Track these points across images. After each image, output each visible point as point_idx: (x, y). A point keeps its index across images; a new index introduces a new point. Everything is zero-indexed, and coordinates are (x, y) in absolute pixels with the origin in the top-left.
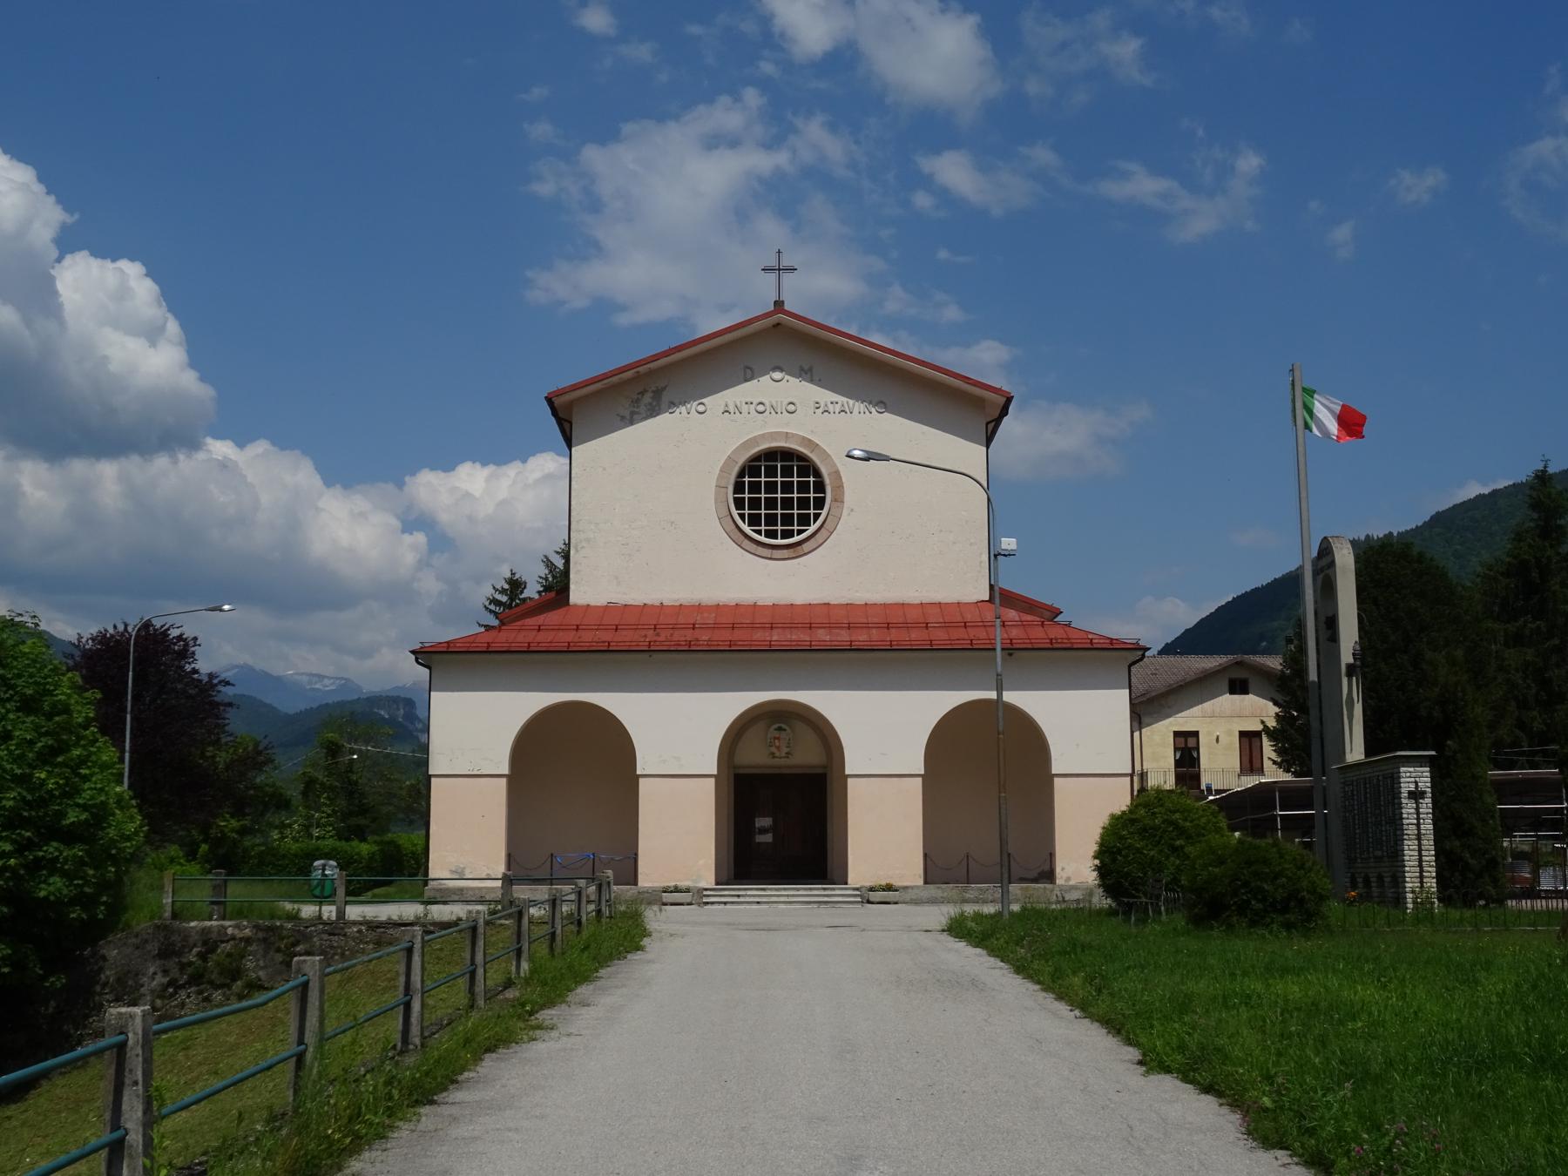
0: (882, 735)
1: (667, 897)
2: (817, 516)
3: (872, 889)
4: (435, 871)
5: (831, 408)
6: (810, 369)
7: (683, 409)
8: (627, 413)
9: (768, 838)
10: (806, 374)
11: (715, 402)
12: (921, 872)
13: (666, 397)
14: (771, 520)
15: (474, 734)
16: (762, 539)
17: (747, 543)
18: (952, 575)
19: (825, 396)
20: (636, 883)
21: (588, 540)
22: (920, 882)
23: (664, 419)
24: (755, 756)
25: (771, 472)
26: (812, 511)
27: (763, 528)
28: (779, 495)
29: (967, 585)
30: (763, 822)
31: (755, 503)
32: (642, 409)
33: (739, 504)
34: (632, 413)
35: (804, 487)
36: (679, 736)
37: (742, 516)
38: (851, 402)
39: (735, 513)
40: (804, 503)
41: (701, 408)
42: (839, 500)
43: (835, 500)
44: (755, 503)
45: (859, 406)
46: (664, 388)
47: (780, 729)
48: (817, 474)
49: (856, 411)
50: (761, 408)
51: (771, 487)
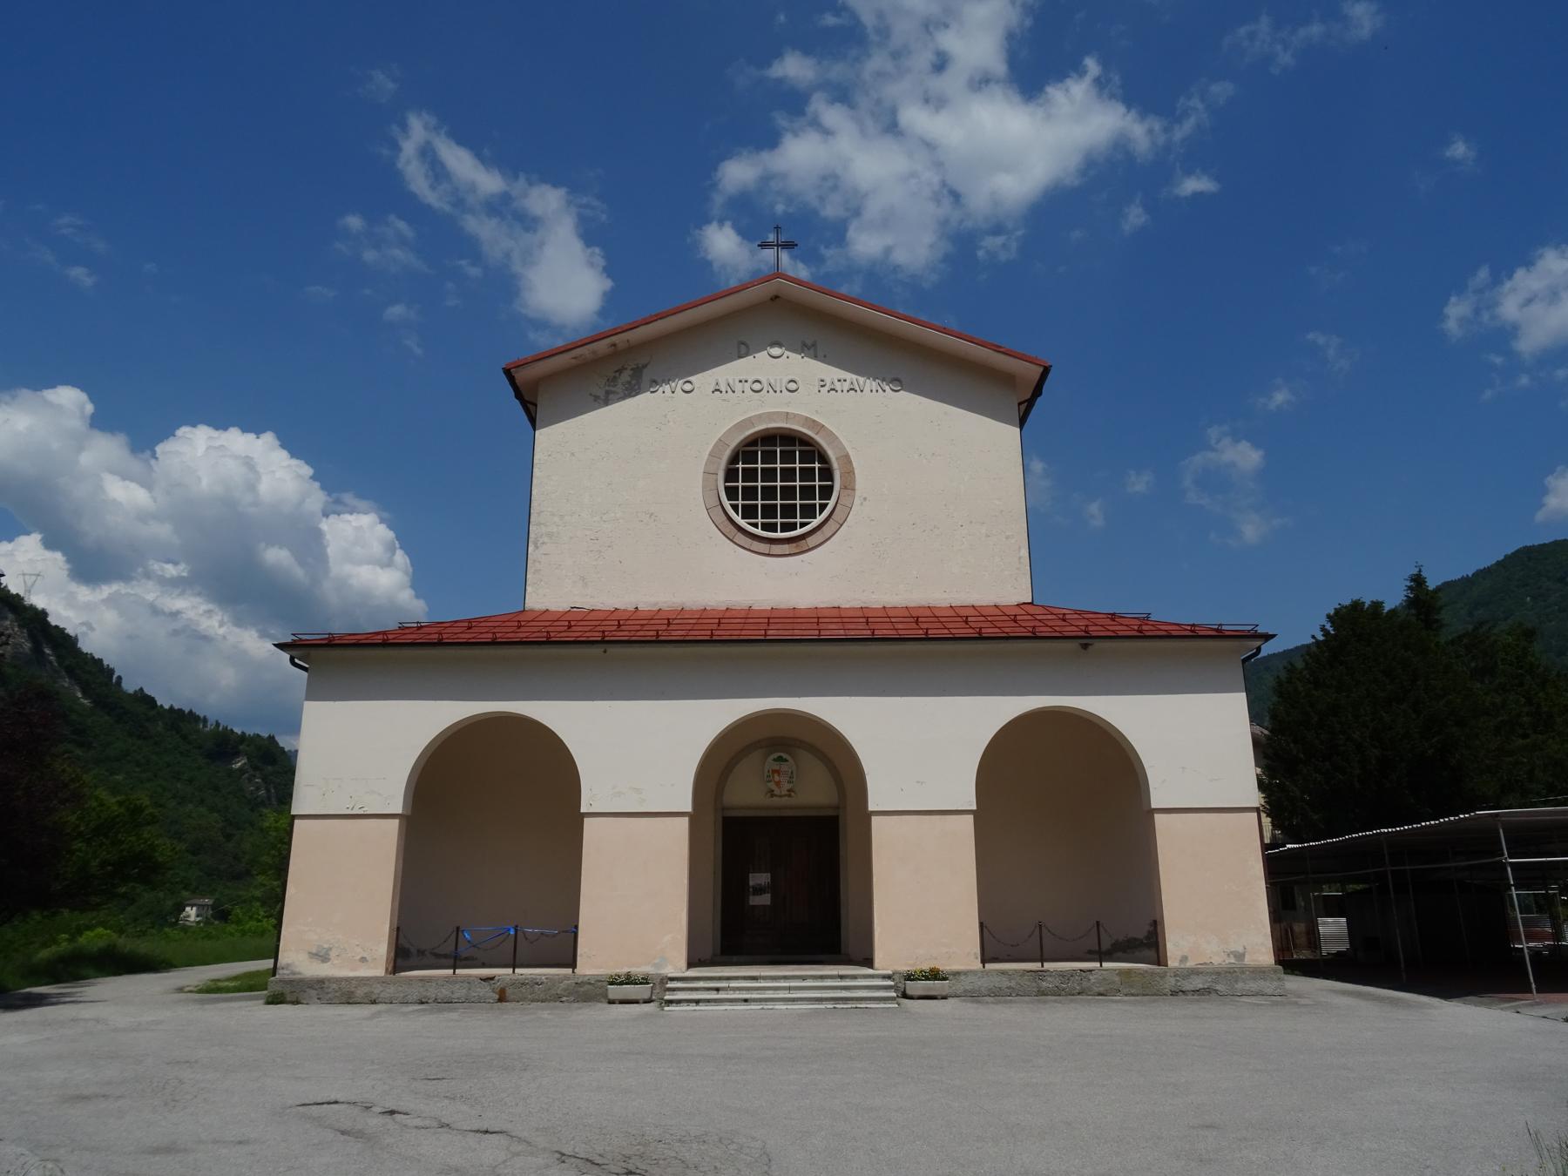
0: (919, 757)
1: (615, 991)
2: (823, 507)
3: (909, 977)
5: (838, 386)
6: (814, 345)
7: (667, 388)
8: (601, 393)
9: (765, 900)
10: (808, 349)
11: (703, 381)
12: (978, 950)
13: (647, 375)
14: (769, 511)
15: (358, 759)
16: (759, 532)
17: (740, 538)
18: (988, 569)
19: (832, 373)
20: (573, 965)
21: (550, 535)
23: (643, 400)
24: (749, 793)
25: (769, 457)
26: (817, 502)
27: (760, 520)
28: (779, 482)
30: (760, 878)
31: (750, 493)
32: (619, 388)
33: (731, 493)
34: (608, 393)
35: (807, 474)
36: (639, 759)
37: (735, 508)
38: (861, 380)
39: (727, 504)
40: (808, 492)
41: (688, 387)
42: (849, 486)
43: (844, 487)
44: (750, 493)
45: (870, 384)
46: (645, 366)
47: (780, 759)
48: (823, 458)
49: (867, 390)
50: (757, 386)
51: (769, 474)
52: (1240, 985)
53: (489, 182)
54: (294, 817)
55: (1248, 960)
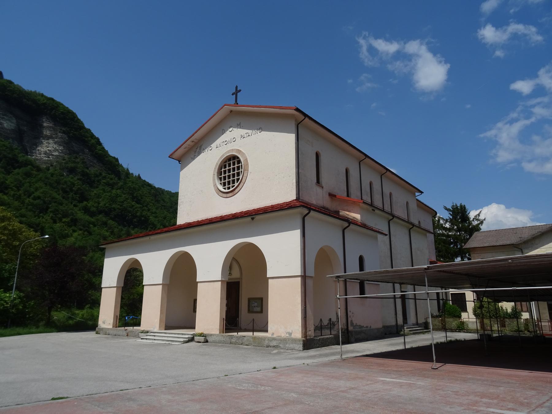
4: (100, 323)
8: (192, 156)
10: (239, 126)
11: (214, 145)
19: (250, 131)
22: (218, 332)
29: (290, 195)
30: (53, 158)
37: (233, 187)
45: (254, 132)
52: (287, 345)
53: (392, 48)
54: (198, 282)
55: (293, 336)
